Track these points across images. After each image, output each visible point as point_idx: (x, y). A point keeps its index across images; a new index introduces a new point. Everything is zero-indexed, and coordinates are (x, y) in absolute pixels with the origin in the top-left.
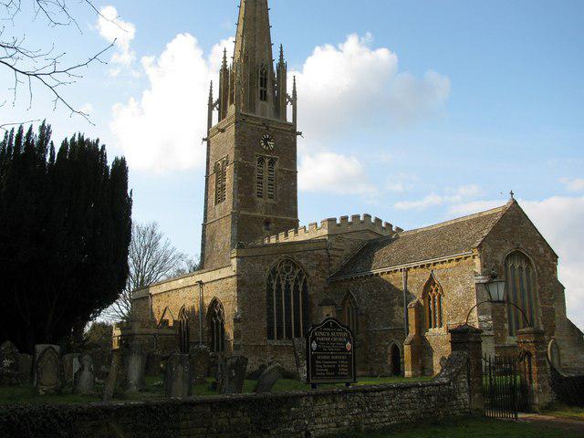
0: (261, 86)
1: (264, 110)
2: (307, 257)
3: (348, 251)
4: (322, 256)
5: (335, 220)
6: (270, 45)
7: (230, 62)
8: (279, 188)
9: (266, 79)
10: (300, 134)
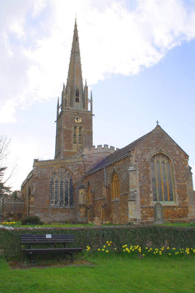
0: (76, 96)
1: (77, 106)
2: (73, 166)
3: (95, 162)
4: (81, 165)
8: (84, 139)
9: (78, 93)
10: (94, 115)
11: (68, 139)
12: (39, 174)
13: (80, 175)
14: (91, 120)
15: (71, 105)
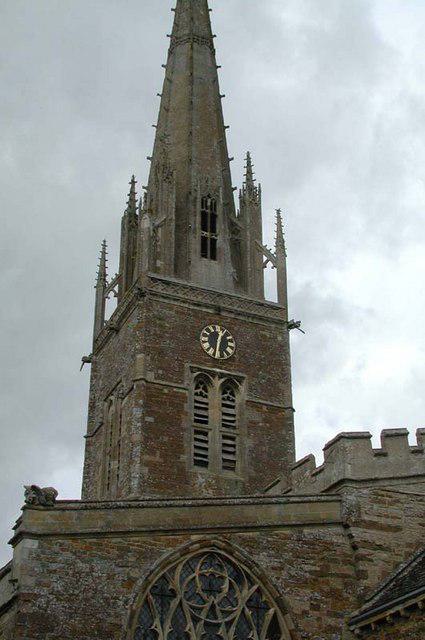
0: (204, 228)
2: (278, 549)
4: (328, 546)
5: (367, 437)
6: (225, 160)
7: (140, 194)
9: (214, 217)
11: (166, 439)
12: (58, 596)
13: (329, 614)
14: (284, 347)
15: (180, 265)
